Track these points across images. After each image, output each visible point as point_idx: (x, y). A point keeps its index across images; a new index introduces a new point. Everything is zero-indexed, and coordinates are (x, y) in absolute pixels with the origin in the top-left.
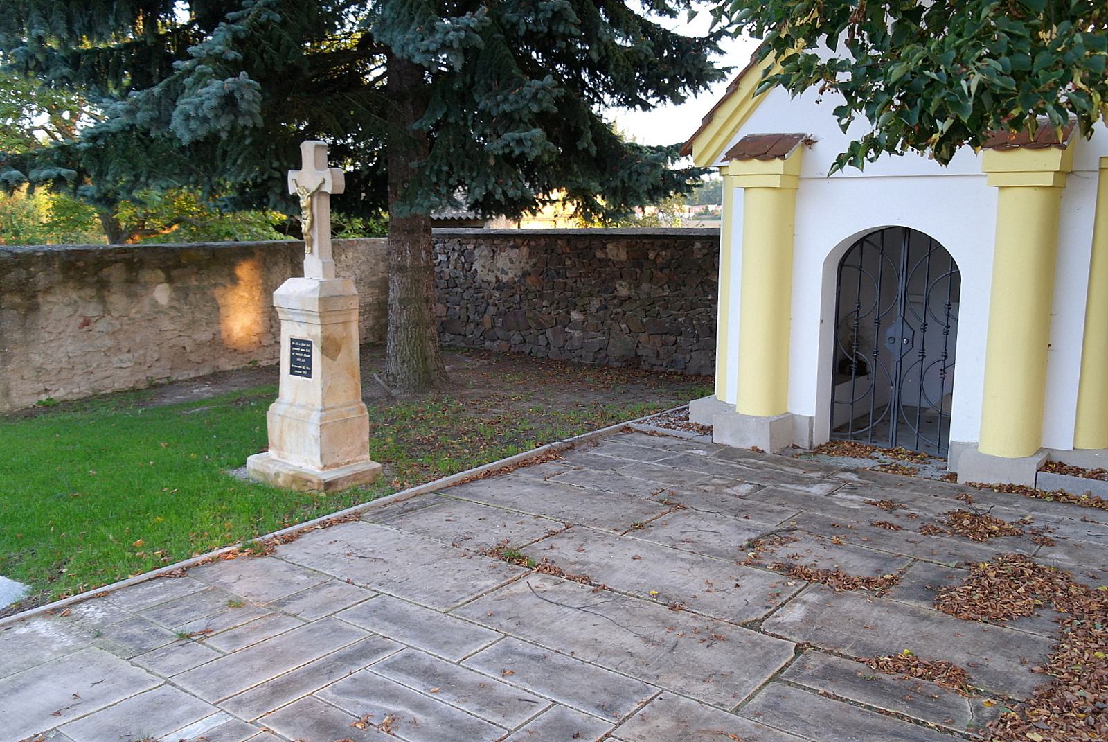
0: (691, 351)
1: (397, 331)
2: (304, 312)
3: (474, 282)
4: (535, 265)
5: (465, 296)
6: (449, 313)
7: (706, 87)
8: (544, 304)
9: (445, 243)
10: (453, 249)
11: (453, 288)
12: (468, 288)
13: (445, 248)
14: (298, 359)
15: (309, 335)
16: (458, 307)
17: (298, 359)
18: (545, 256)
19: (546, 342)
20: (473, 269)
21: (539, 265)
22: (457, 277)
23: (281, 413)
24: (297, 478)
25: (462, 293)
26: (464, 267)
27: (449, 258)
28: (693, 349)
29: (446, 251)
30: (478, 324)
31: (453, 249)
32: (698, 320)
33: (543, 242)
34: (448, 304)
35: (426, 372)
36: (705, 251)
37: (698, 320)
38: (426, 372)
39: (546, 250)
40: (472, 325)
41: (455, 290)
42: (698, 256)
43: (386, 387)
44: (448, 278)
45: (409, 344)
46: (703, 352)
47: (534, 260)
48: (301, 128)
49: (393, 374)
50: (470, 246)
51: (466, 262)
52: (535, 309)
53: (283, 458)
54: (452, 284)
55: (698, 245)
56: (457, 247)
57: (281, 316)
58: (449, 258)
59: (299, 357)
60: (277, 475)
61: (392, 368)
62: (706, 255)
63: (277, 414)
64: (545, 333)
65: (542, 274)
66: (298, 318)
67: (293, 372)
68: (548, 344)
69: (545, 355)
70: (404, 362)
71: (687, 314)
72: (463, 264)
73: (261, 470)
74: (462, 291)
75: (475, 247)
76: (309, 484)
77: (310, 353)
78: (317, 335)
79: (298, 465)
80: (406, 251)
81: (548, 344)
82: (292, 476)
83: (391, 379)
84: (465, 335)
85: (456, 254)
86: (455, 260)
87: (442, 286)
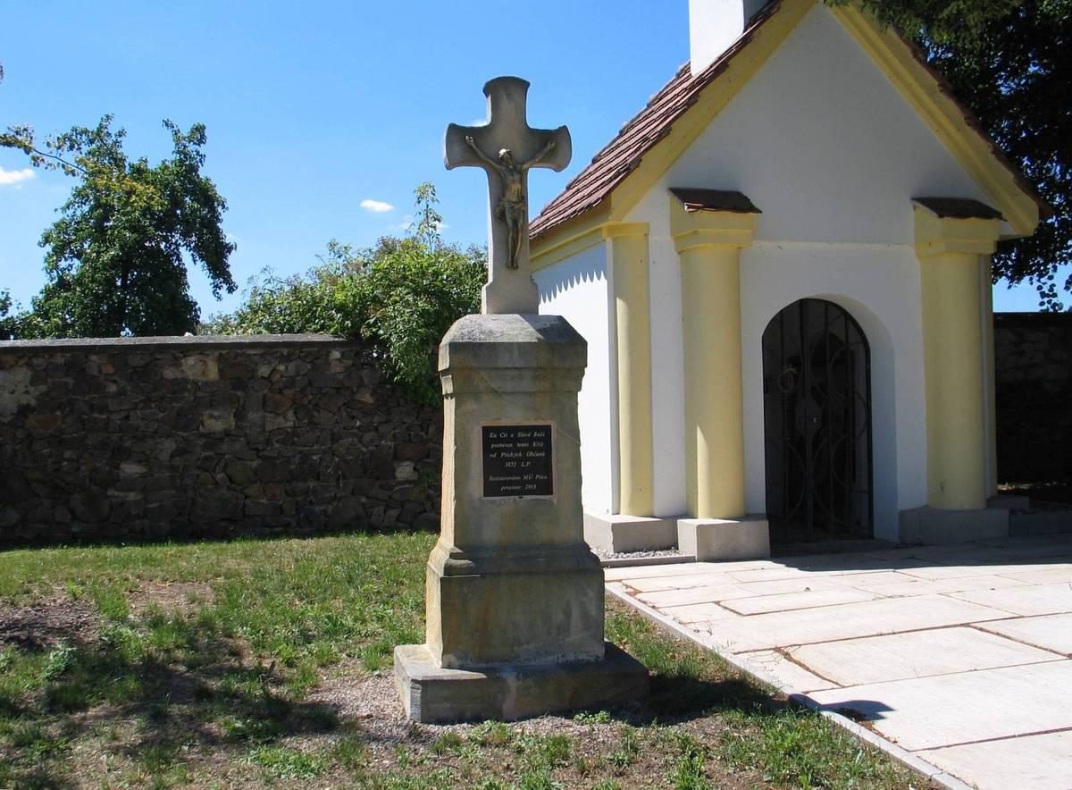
14: (508, 464)
17: (508, 464)
77: (548, 449)
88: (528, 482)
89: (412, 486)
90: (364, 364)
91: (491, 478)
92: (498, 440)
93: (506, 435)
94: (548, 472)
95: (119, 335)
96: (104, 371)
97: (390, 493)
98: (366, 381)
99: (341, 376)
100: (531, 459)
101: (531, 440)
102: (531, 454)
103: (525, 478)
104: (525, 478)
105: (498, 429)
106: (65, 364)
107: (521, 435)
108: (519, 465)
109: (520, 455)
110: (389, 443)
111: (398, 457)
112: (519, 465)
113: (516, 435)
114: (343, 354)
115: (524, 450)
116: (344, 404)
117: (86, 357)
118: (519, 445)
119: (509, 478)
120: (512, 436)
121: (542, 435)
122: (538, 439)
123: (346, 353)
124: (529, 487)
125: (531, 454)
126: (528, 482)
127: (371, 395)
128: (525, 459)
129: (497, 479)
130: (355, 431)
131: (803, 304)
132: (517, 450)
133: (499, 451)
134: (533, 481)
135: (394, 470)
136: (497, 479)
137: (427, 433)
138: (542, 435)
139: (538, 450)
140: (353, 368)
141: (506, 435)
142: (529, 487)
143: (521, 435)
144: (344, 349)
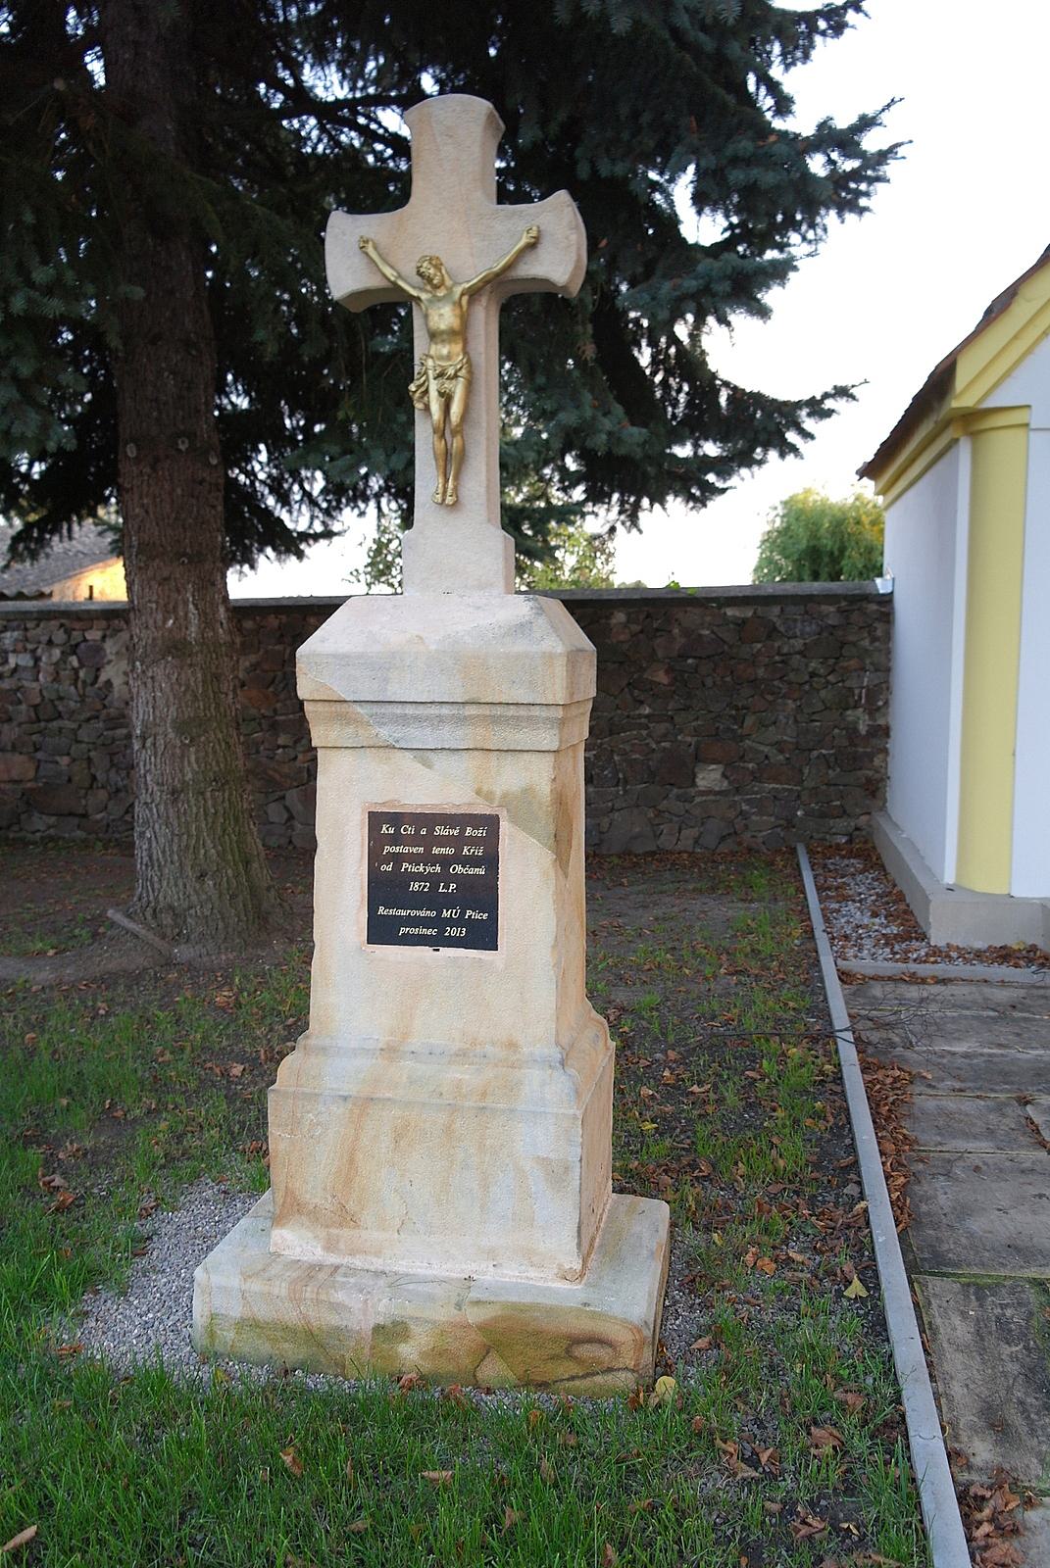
0: (612, 810)
1: (175, 801)
2: (471, 711)
3: (105, 707)
4: (255, 667)
5: (83, 735)
6: (42, 772)
7: (723, 320)
8: (280, 741)
9: (26, 629)
10: (50, 642)
11: (48, 721)
12: (88, 720)
13: (27, 640)
14: (415, 886)
15: (488, 797)
16: (64, 761)
17: (415, 886)
18: (279, 647)
19: (286, 816)
20: (103, 678)
21: (266, 667)
22: (61, 698)
23: (349, 1088)
24: (509, 1333)
25: (74, 732)
26: (77, 678)
27: (37, 660)
28: (617, 806)
29: (30, 646)
30: (118, 791)
31: (50, 642)
32: (624, 753)
33: (273, 621)
34: (39, 755)
35: (253, 891)
36: (635, 628)
37: (624, 753)
38: (253, 891)
39: (282, 636)
40: (102, 795)
41: (55, 724)
42: (622, 637)
43: (157, 941)
44: (38, 701)
45: (212, 829)
46: (636, 811)
47: (253, 658)
48: (404, 92)
49: (171, 907)
50: (94, 635)
51: (82, 665)
52: (258, 752)
53: (352, 1253)
54: (46, 712)
55: (620, 617)
56: (60, 636)
57: (318, 736)
58: (37, 660)
59: (419, 877)
60: (391, 1332)
61: (170, 893)
62: (636, 635)
63: (314, 1097)
64: (283, 798)
65: (273, 682)
66: (448, 736)
67: (381, 932)
68: (291, 817)
69: (283, 841)
70: (202, 876)
71: (601, 744)
72: (76, 671)
73: (291, 1316)
74: (74, 726)
75: (104, 638)
76: (584, 1351)
77: (491, 861)
78: (528, 792)
79: (457, 1270)
80: (186, 603)
81: (291, 817)
82: (482, 1328)
83: (167, 919)
84: (85, 816)
85: (57, 653)
86: (56, 664)
87: (23, 718)
88: (451, 922)
89: (718, 797)
90: (657, 630)
91: (381, 910)
92: (396, 840)
93: (411, 830)
94: (492, 907)
95: (839, 580)
96: (28, 656)
97: (688, 806)
98: (660, 654)
99: (626, 646)
100: (456, 878)
101: (459, 841)
102: (459, 869)
103: (446, 914)
104: (446, 914)
105: (396, 819)
106: (280, 628)
107: (439, 831)
108: (434, 887)
109: (438, 869)
110: (689, 739)
111: (699, 758)
112: (434, 887)
113: (431, 831)
114: (629, 615)
115: (445, 862)
116: (629, 684)
117: (304, 619)
118: (436, 851)
119: (413, 913)
120: (423, 832)
121: (481, 833)
122: (474, 841)
123: (633, 616)
124: (453, 932)
125: (459, 869)
126: (451, 922)
127: (667, 672)
128: (448, 878)
129: (392, 912)
130: (643, 720)
131: (407, 202)
132: (428, 859)
133: (397, 859)
134: (458, 923)
135: (694, 776)
136: (392, 912)
137: (741, 727)
138: (481, 833)
139: (474, 862)
140: (641, 636)
141: (411, 830)
142: (453, 932)
143: (439, 831)
144: (631, 610)
